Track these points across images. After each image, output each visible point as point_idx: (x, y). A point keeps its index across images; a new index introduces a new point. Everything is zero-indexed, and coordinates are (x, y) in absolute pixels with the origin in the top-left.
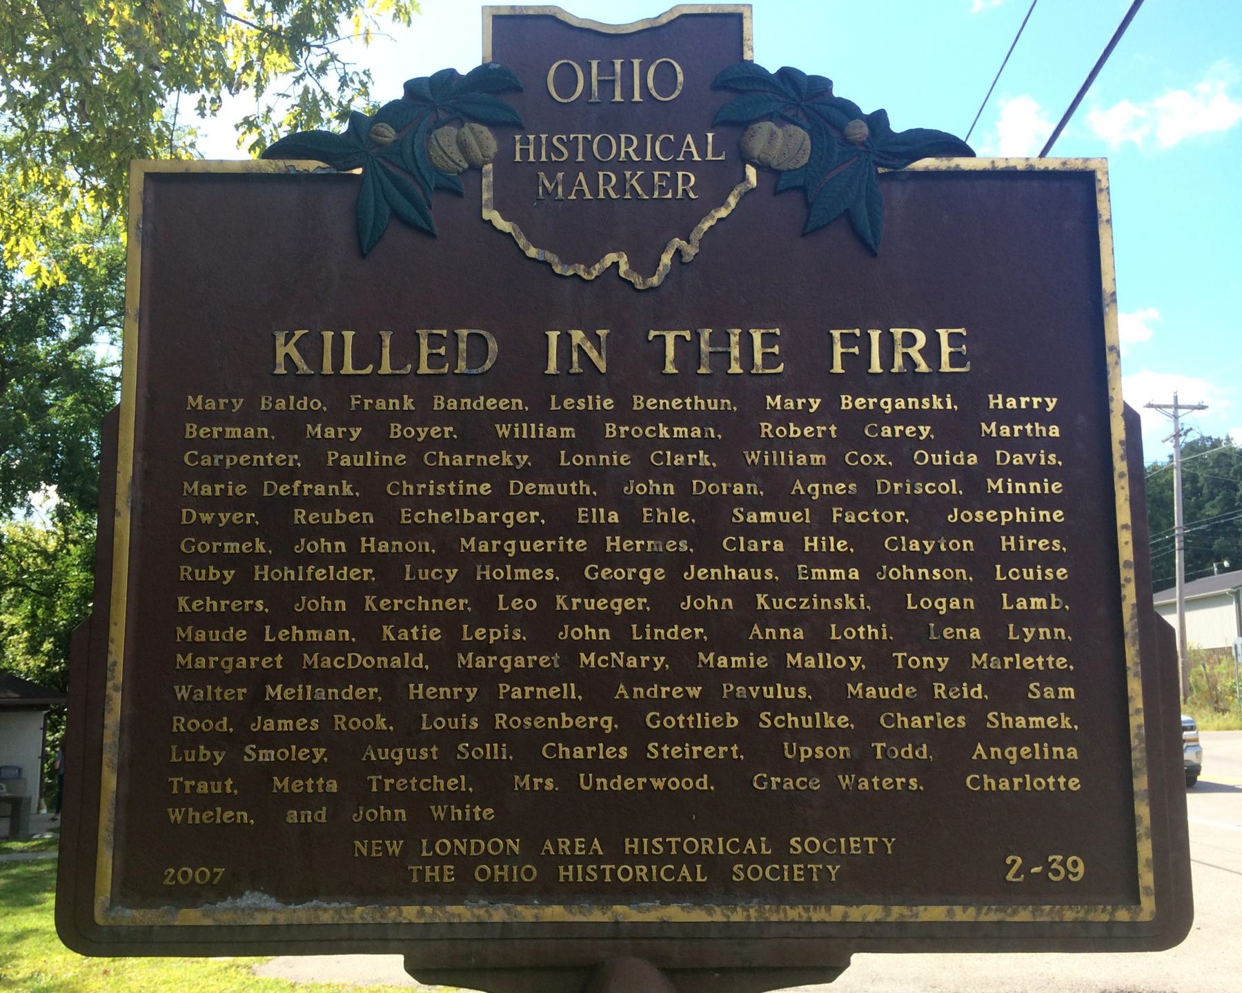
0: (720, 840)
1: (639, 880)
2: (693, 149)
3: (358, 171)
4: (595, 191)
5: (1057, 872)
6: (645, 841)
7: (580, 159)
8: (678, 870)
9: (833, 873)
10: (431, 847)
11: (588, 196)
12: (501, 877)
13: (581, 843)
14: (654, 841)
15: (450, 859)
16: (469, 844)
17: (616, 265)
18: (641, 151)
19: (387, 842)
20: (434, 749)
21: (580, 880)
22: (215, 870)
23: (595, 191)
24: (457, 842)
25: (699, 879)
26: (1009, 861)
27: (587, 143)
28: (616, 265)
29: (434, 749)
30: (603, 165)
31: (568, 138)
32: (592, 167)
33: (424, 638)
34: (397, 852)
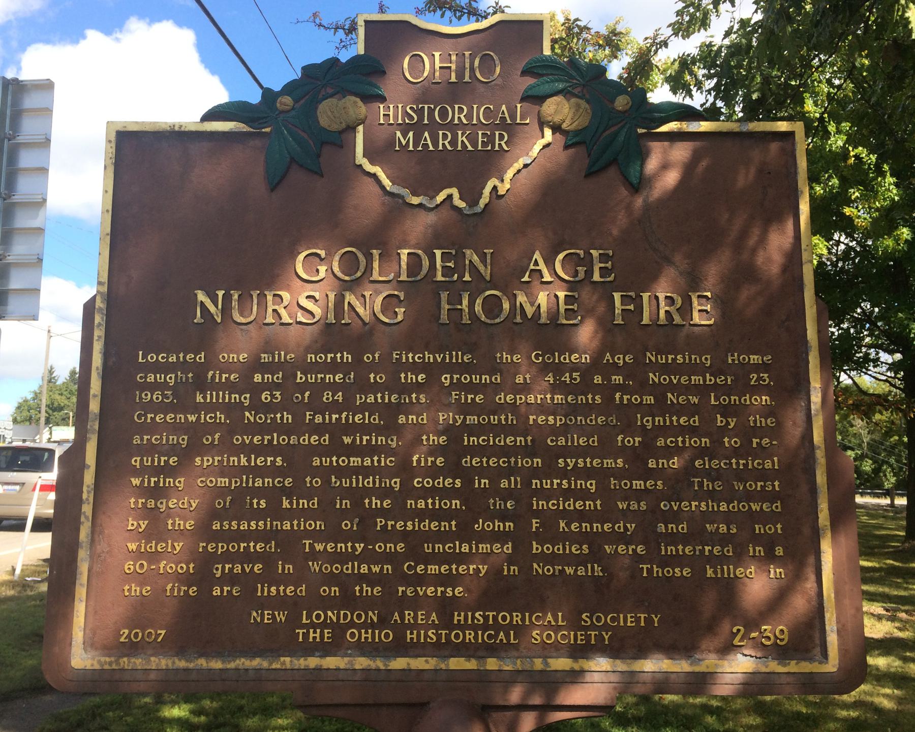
0: (527, 614)
1: (467, 641)
2: (507, 115)
3: (268, 130)
4: (435, 144)
5: (768, 638)
6: (470, 614)
7: (426, 122)
8: (497, 634)
9: (606, 637)
10: (309, 617)
11: (431, 148)
12: (366, 638)
13: (422, 614)
14: (477, 615)
15: (324, 625)
16: (338, 614)
17: (450, 197)
18: (469, 116)
19: (276, 613)
20: (453, 523)
21: (470, 622)
22: (159, 632)
23: (435, 144)
24: (330, 613)
25: (512, 641)
26: (735, 630)
27: (431, 111)
28: (450, 197)
29: (453, 523)
30: (442, 127)
31: (417, 107)
32: (433, 127)
33: (383, 464)
34: (283, 619)
